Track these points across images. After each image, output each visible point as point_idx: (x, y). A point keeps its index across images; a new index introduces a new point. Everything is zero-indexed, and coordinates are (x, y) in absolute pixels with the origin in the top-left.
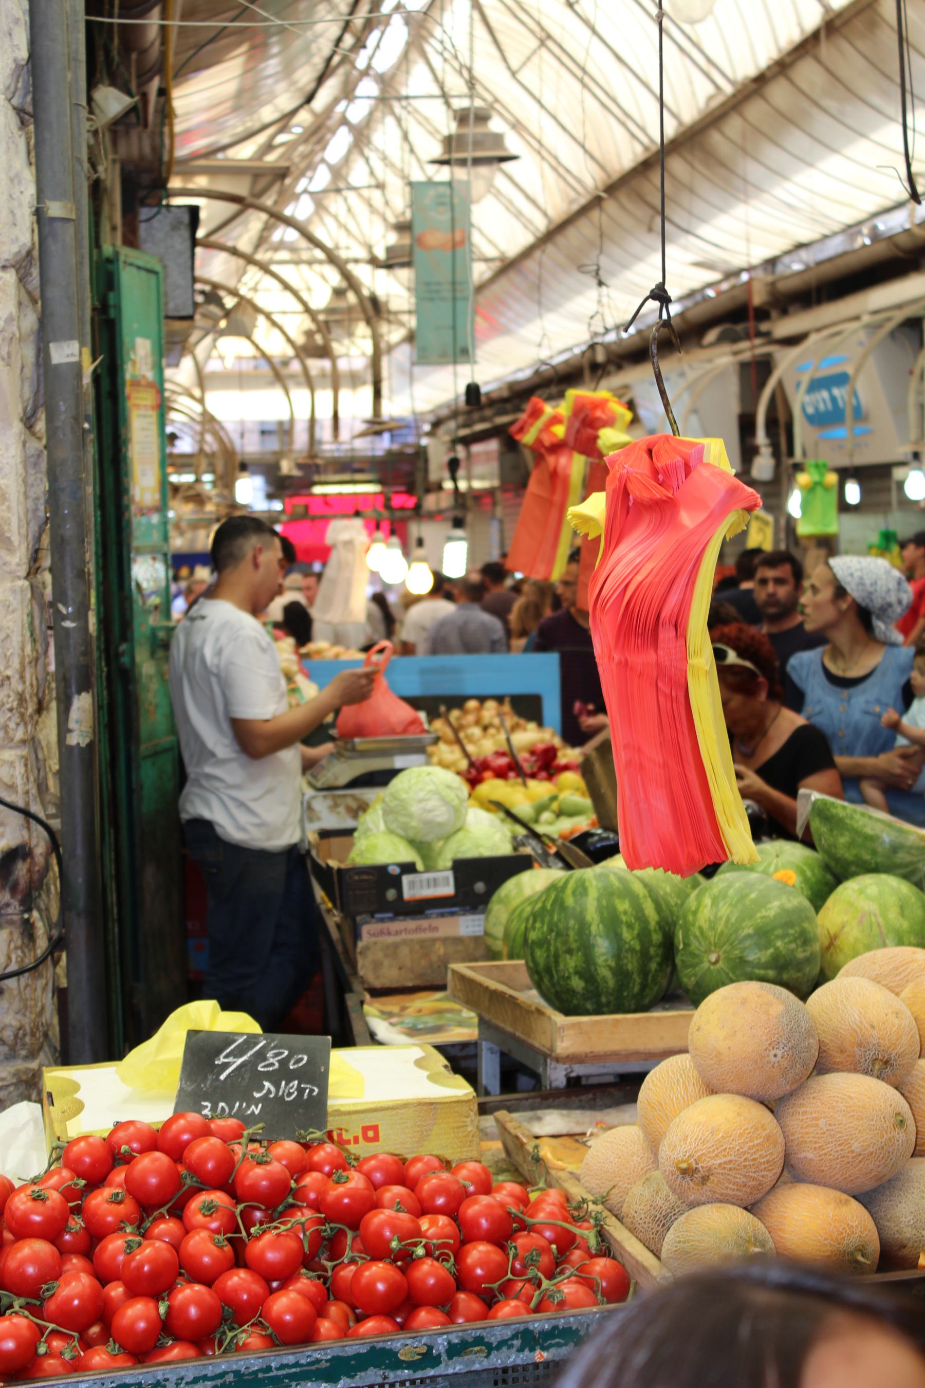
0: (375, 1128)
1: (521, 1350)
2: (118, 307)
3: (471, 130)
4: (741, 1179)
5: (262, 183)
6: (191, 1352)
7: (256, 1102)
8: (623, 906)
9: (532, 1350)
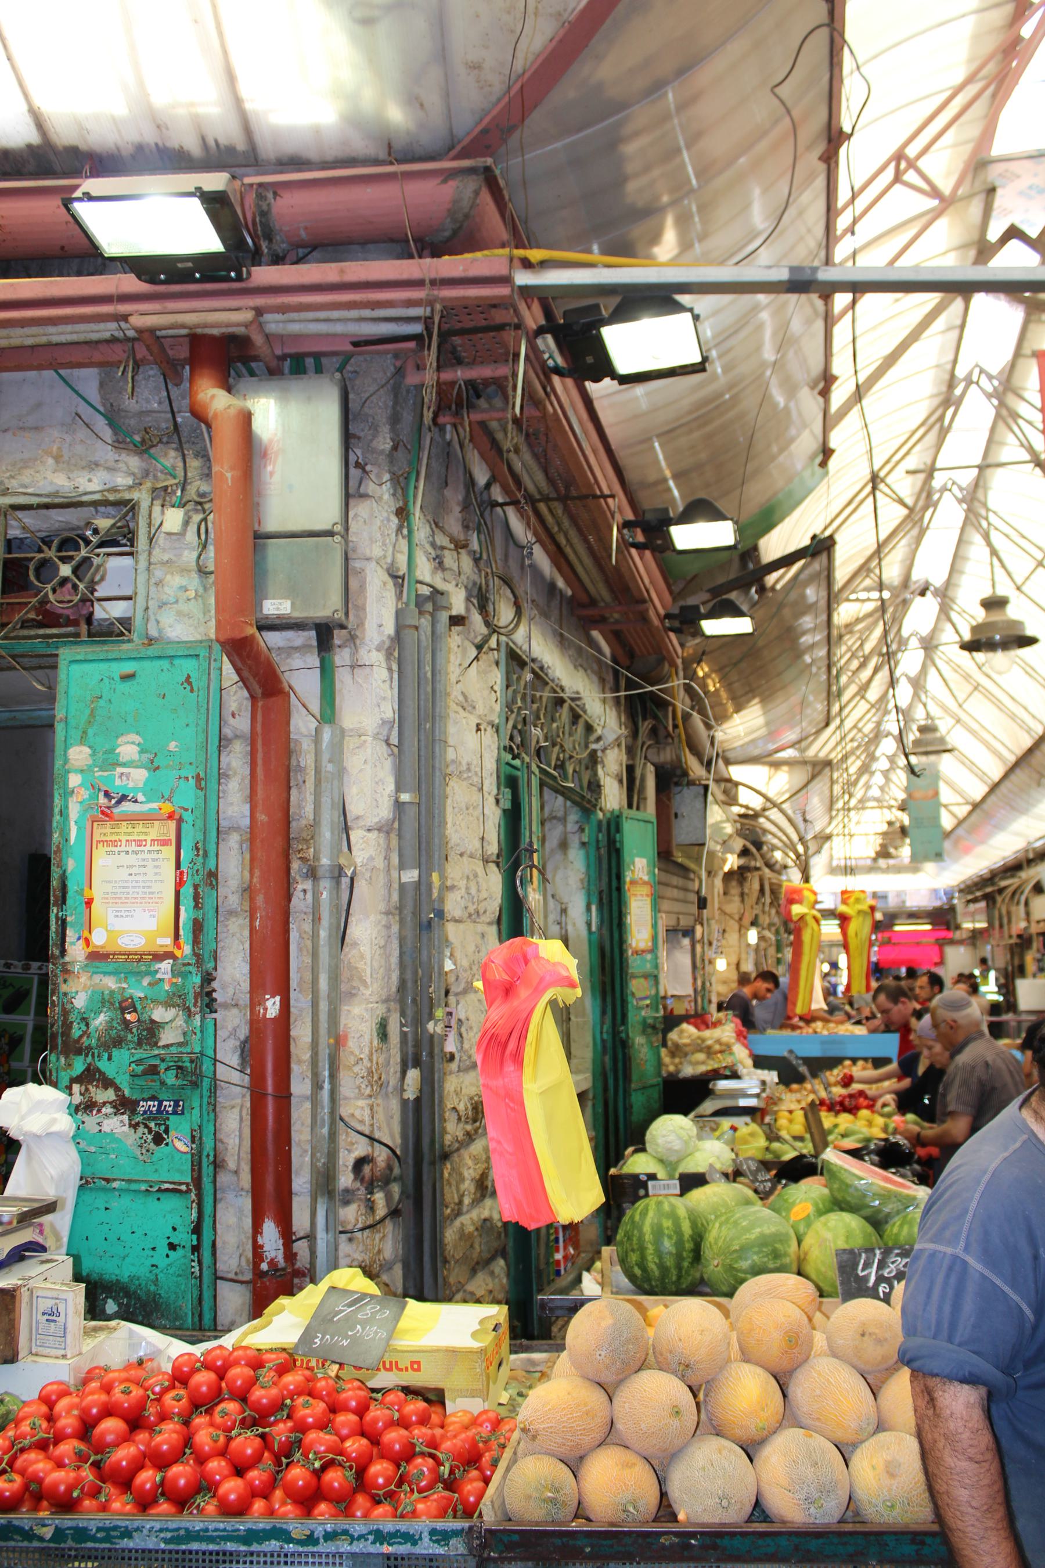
0: (418, 1363)
1: (374, 1543)
2: (622, 842)
3: (929, 736)
4: (560, 1440)
5: (817, 769)
6: (173, 1510)
7: (346, 1337)
8: (667, 1223)
9: (381, 1544)
